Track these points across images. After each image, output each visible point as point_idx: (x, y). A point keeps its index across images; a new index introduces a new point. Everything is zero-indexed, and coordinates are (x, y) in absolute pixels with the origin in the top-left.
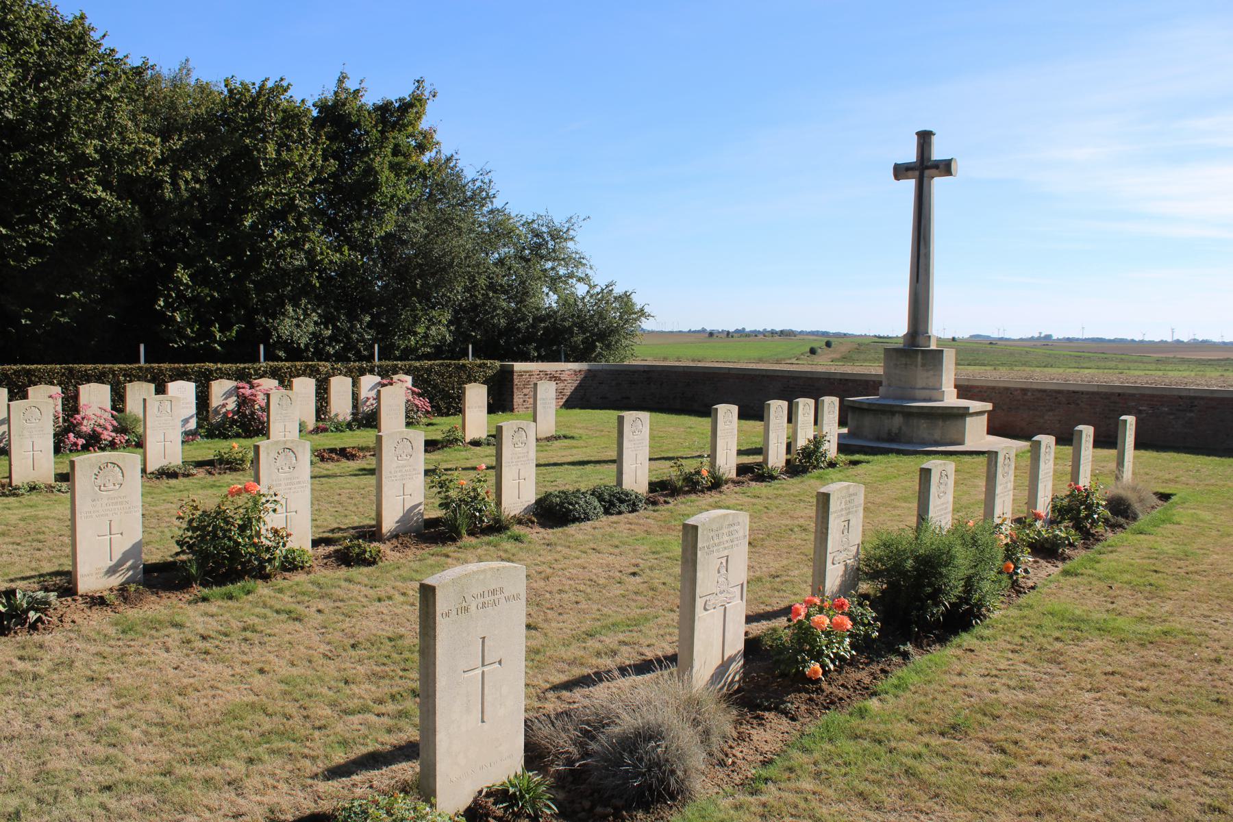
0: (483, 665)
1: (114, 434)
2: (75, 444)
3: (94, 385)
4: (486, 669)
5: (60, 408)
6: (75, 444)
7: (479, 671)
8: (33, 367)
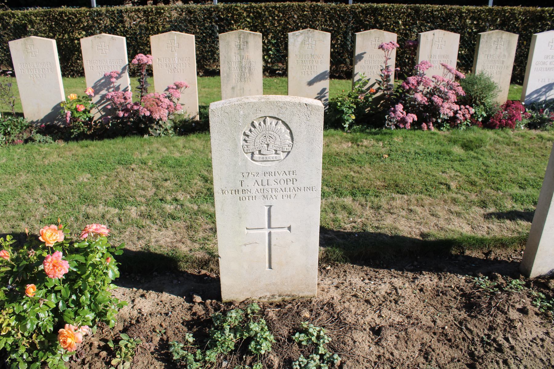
0: (269, 227)
1: (456, 107)
2: (403, 121)
3: (439, 33)
4: (273, 231)
5: (392, 63)
6: (403, 121)
7: (266, 232)
8: (380, 5)
